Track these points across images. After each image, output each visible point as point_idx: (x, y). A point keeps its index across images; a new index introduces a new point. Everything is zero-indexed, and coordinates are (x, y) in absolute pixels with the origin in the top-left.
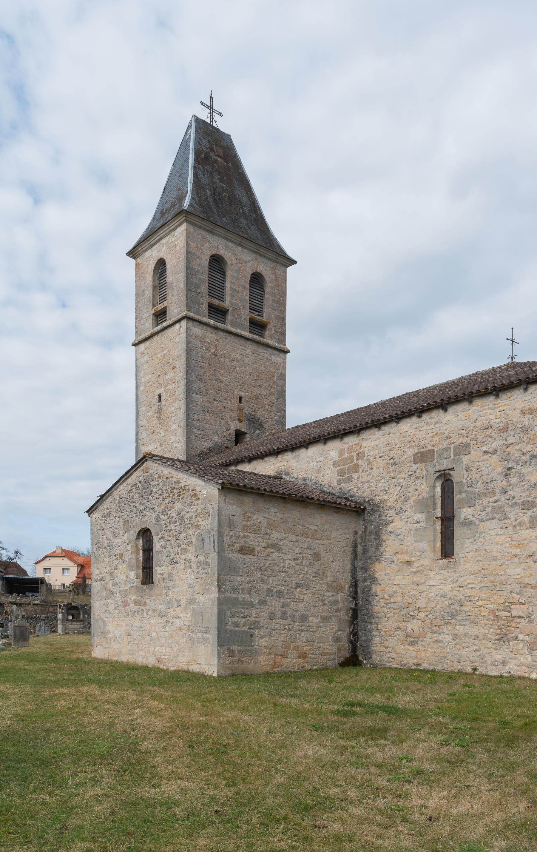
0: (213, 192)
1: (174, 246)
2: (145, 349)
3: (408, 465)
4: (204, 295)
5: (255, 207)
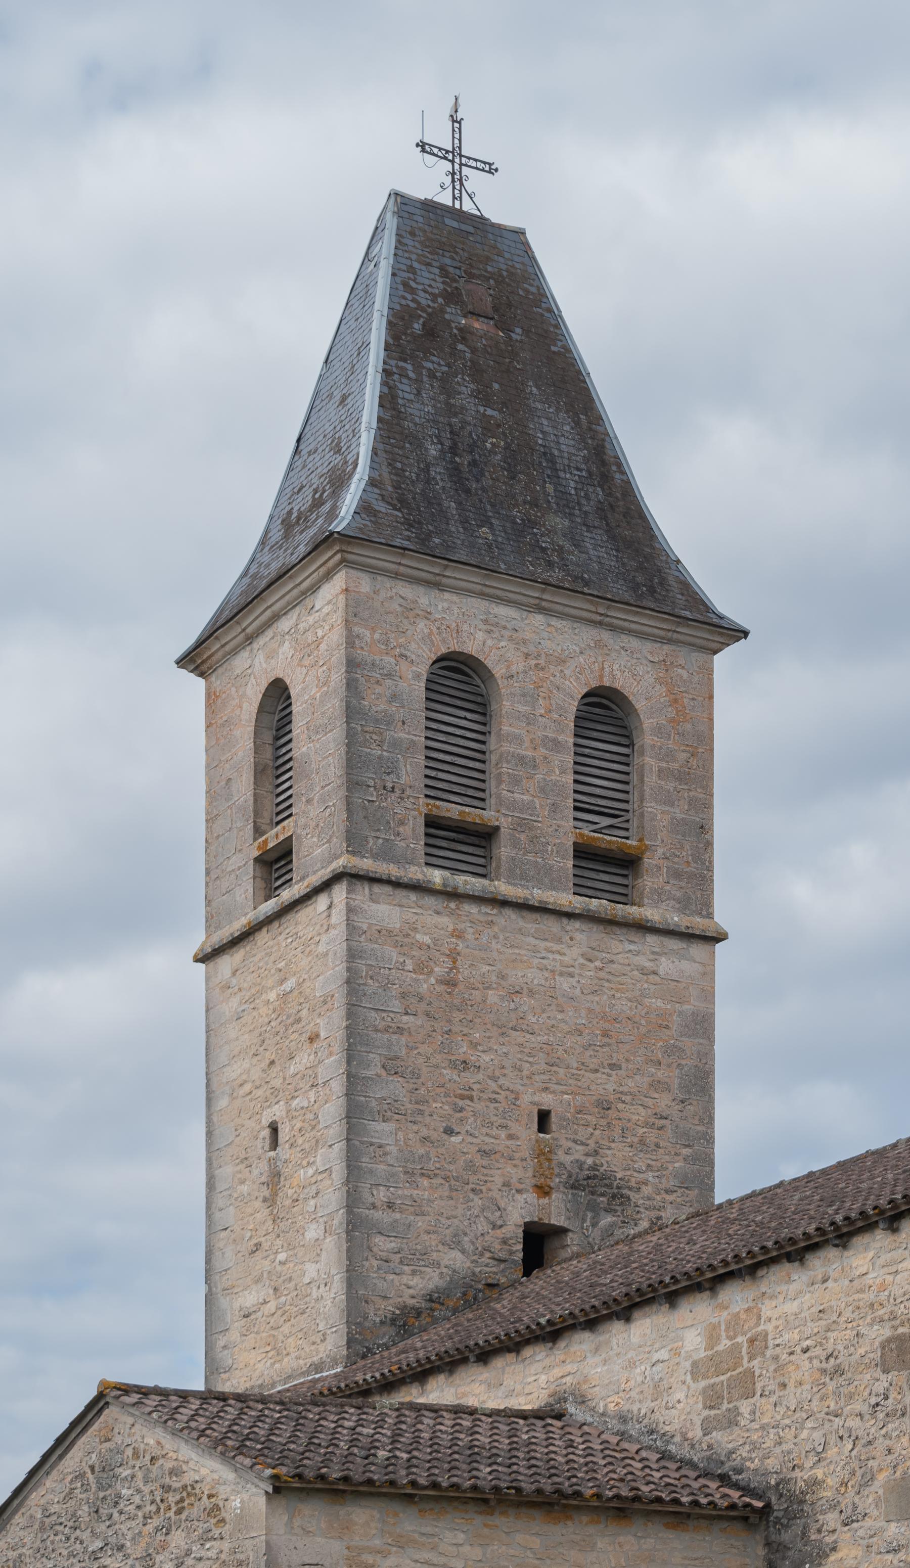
0: (448, 443)
1: (307, 645)
2: (234, 973)
3: (868, 1376)
4: (408, 792)
5: (604, 463)
